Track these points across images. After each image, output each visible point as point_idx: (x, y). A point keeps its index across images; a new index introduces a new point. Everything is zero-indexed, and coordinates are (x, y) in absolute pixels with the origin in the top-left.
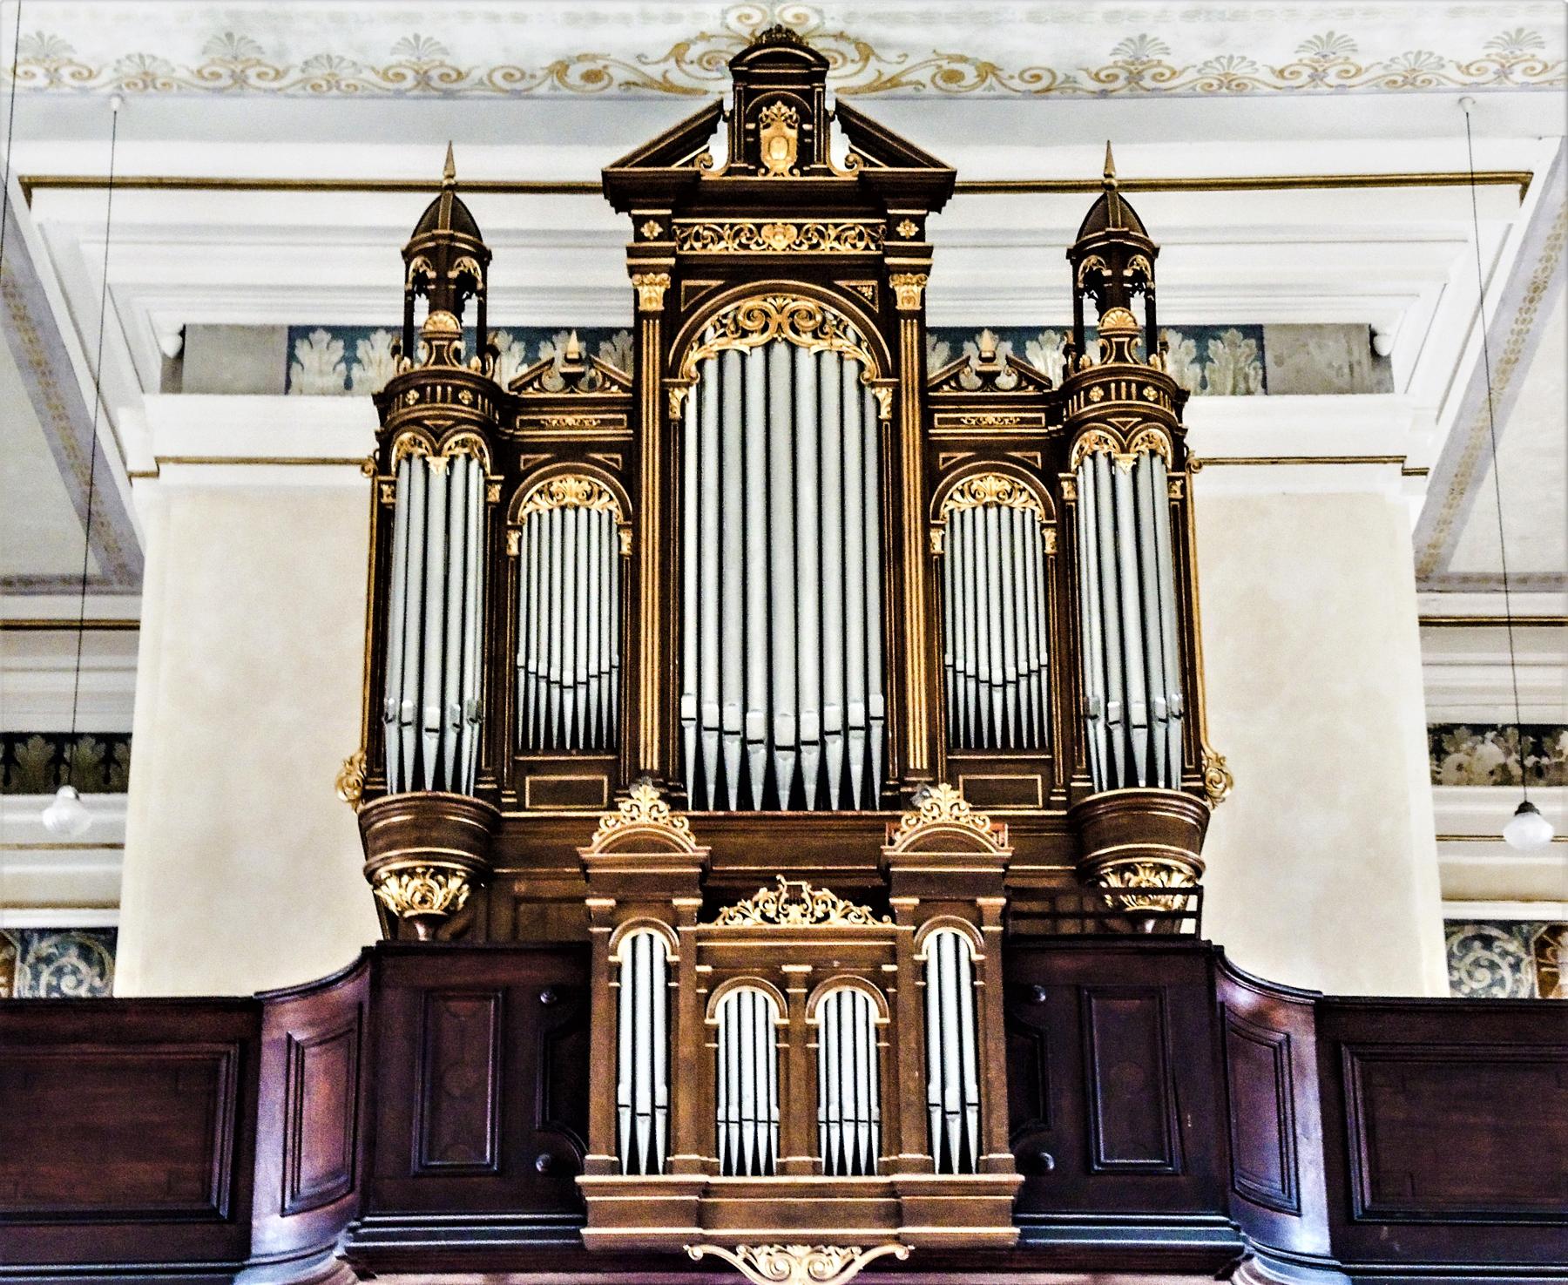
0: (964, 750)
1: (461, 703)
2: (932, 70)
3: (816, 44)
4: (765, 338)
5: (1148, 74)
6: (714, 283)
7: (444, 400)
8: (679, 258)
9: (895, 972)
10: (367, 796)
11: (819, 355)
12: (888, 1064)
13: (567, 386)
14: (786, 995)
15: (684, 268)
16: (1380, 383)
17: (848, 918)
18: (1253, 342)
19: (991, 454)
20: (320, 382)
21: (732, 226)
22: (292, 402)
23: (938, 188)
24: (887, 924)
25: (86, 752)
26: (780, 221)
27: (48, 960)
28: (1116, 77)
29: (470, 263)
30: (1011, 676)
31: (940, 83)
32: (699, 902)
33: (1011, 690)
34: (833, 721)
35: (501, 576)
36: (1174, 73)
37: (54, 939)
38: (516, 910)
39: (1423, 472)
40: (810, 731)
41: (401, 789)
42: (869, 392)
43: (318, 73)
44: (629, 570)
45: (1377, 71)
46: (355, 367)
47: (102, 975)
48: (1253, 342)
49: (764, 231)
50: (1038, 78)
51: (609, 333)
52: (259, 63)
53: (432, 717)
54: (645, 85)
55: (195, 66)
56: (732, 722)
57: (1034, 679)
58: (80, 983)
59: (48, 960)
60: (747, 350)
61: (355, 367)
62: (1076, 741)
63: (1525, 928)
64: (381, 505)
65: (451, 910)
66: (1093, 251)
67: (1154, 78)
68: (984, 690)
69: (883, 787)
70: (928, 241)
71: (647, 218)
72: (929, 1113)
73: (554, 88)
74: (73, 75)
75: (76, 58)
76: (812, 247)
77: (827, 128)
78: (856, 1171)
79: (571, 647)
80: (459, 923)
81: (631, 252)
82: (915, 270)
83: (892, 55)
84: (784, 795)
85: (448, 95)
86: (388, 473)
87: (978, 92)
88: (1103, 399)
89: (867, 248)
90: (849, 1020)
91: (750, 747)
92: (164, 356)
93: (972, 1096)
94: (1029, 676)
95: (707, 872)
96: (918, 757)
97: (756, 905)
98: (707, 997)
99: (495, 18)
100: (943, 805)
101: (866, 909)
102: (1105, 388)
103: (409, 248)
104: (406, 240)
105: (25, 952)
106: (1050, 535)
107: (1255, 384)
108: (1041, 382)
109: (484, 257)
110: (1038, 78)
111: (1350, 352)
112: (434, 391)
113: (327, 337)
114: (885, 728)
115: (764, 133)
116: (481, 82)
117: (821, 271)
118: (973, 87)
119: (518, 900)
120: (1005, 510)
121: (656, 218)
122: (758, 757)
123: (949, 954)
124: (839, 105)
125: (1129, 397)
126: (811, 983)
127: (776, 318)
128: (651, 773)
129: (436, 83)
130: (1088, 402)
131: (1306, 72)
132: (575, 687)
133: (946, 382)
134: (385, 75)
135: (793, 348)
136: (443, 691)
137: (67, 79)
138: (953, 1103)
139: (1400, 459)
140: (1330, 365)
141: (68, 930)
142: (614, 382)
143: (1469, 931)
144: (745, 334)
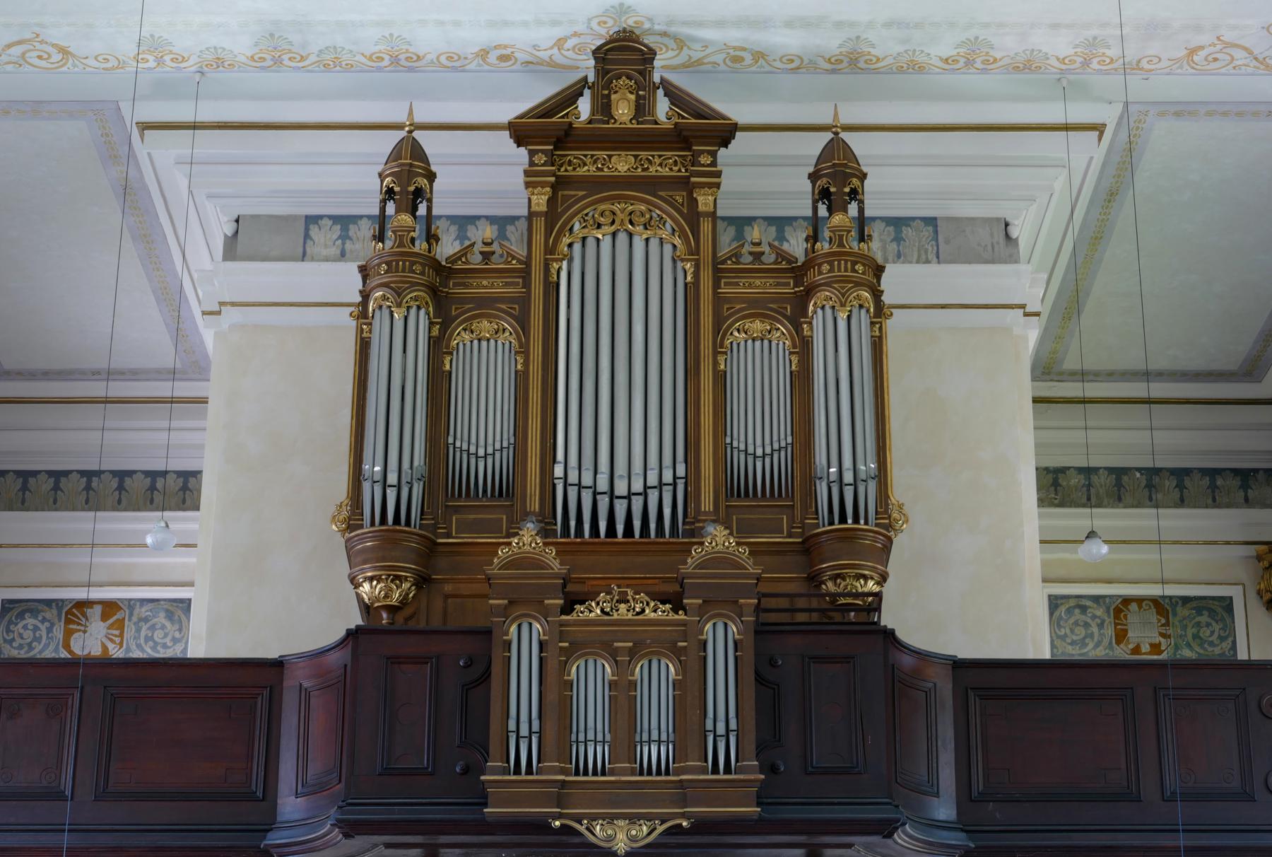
0: (736, 492)
1: (411, 468)
2: (723, 56)
3: (648, 40)
4: (613, 228)
5: (862, 60)
6: (581, 193)
7: (403, 271)
8: (557, 177)
9: (685, 647)
10: (350, 528)
11: (647, 240)
12: (679, 706)
13: (484, 259)
14: (616, 662)
15: (560, 184)
16: (1011, 256)
17: (661, 613)
18: (930, 228)
19: (758, 308)
20: (324, 252)
21: (592, 156)
22: (307, 266)
23: (725, 133)
24: (681, 616)
25: (173, 483)
26: (623, 153)
27: (146, 620)
28: (842, 61)
29: (423, 182)
30: (768, 450)
31: (727, 61)
32: (561, 602)
33: (768, 460)
34: (652, 479)
35: (439, 386)
36: (878, 59)
37: (150, 606)
38: (445, 602)
39: (1037, 314)
40: (638, 486)
41: (373, 524)
42: (680, 265)
43: (328, 57)
44: (521, 380)
45: (1006, 61)
46: (348, 242)
47: (180, 630)
48: (930, 228)
49: (613, 159)
50: (792, 61)
51: (513, 219)
52: (290, 52)
53: (392, 478)
54: (538, 63)
55: (249, 54)
56: (587, 480)
57: (783, 453)
58: (166, 635)
59: (146, 620)
60: (600, 236)
61: (348, 242)
62: (811, 494)
63: (1107, 600)
64: (362, 339)
65: (404, 602)
66: (825, 175)
67: (866, 62)
68: (750, 459)
69: (684, 523)
70: (719, 168)
71: (537, 151)
72: (706, 737)
73: (480, 65)
74: (172, 60)
75: (175, 50)
76: (644, 170)
77: (654, 93)
78: (659, 773)
79: (484, 426)
80: (407, 611)
81: (527, 173)
82: (710, 185)
83: (697, 46)
84: (620, 528)
85: (411, 70)
86: (366, 318)
87: (754, 69)
88: (829, 271)
89: (679, 171)
90: (657, 680)
91: (598, 497)
92: (226, 236)
93: (733, 725)
94: (779, 450)
95: (566, 580)
96: (707, 503)
97: (598, 604)
98: (566, 662)
99: (442, 23)
100: (718, 538)
101: (668, 606)
102: (833, 253)
103: (384, 171)
104: (380, 168)
105: (131, 615)
106: (795, 359)
107: (932, 256)
108: (790, 259)
109: (431, 177)
110: (792, 61)
111: (992, 235)
112: (397, 264)
113: (330, 223)
114: (686, 484)
115: (613, 97)
116: (432, 62)
117: (651, 185)
118: (750, 66)
119: (447, 597)
120: (766, 342)
121: (542, 151)
122: (603, 502)
123: (721, 638)
124: (662, 78)
125: (846, 270)
126: (633, 653)
127: (620, 216)
128: (534, 513)
129: (403, 63)
130: (820, 273)
131: (962, 61)
132: (485, 457)
133: (729, 258)
134: (370, 59)
135: (631, 235)
136: (400, 457)
137: (168, 62)
138: (721, 729)
139: (1023, 306)
140: (979, 245)
141: (158, 600)
142: (514, 258)
143: (1072, 603)
144: (599, 226)
